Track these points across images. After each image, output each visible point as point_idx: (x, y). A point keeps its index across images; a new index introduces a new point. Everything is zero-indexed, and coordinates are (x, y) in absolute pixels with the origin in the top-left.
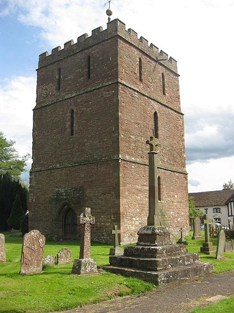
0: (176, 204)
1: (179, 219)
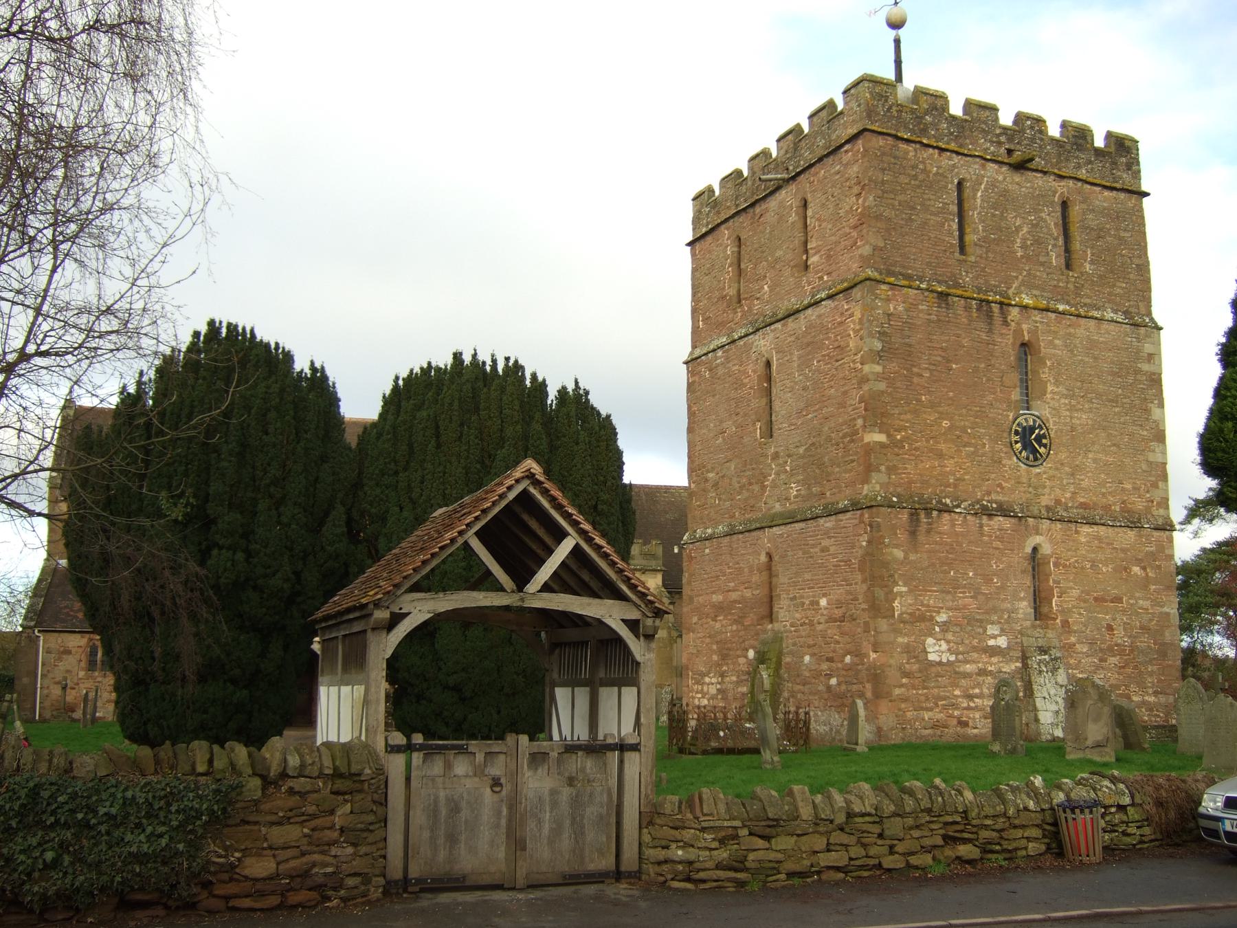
0: (820, 627)
1: (833, 681)
